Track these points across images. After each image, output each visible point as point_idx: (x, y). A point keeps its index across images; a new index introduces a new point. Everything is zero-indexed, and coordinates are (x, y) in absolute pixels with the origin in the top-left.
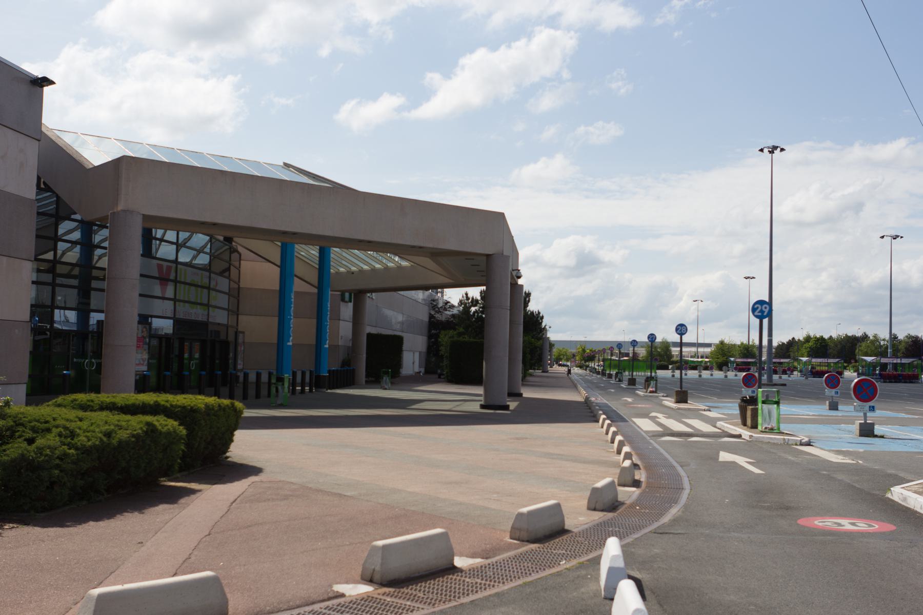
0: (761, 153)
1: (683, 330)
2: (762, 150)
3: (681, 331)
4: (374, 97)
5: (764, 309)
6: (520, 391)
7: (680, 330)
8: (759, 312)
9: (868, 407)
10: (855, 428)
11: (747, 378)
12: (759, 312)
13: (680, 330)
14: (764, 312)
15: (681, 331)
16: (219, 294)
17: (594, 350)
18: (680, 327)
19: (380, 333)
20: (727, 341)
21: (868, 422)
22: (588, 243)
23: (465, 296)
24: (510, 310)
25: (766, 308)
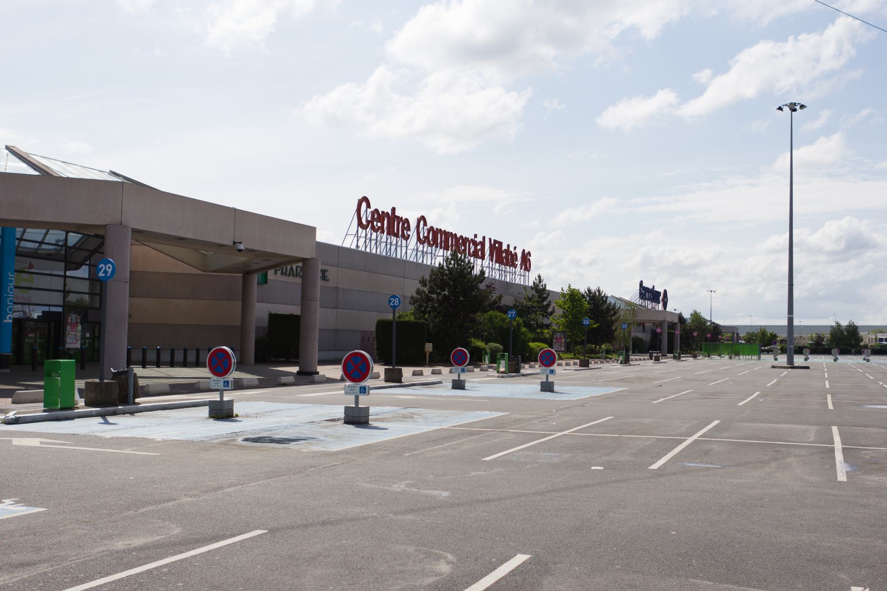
0: (780, 111)
1: (396, 302)
2: (780, 109)
3: (394, 303)
4: (650, 93)
5: (108, 270)
6: (316, 369)
7: (393, 302)
8: (103, 273)
9: (359, 389)
10: (339, 412)
11: (550, 356)
12: (103, 273)
13: (393, 302)
14: (108, 272)
15: (394, 303)
16: (34, 276)
17: (774, 333)
18: (393, 299)
19: (292, 313)
20: (706, 315)
21: (360, 406)
22: (863, 227)
23: (538, 278)
24: (130, 283)
25: (109, 268)
